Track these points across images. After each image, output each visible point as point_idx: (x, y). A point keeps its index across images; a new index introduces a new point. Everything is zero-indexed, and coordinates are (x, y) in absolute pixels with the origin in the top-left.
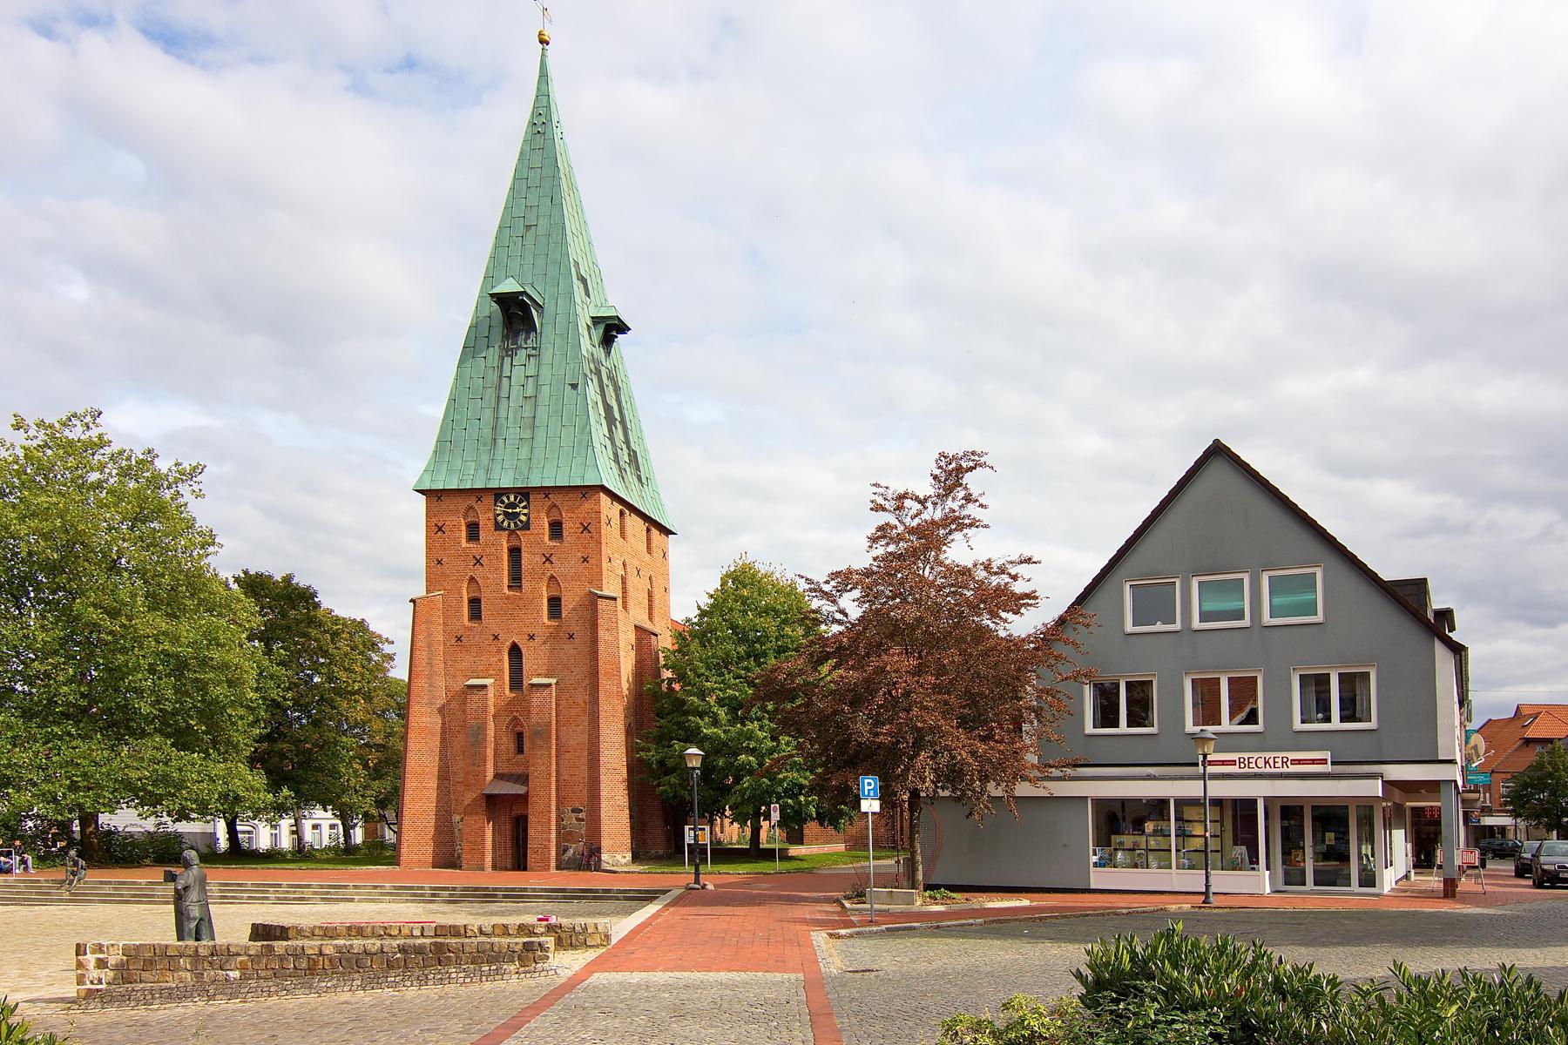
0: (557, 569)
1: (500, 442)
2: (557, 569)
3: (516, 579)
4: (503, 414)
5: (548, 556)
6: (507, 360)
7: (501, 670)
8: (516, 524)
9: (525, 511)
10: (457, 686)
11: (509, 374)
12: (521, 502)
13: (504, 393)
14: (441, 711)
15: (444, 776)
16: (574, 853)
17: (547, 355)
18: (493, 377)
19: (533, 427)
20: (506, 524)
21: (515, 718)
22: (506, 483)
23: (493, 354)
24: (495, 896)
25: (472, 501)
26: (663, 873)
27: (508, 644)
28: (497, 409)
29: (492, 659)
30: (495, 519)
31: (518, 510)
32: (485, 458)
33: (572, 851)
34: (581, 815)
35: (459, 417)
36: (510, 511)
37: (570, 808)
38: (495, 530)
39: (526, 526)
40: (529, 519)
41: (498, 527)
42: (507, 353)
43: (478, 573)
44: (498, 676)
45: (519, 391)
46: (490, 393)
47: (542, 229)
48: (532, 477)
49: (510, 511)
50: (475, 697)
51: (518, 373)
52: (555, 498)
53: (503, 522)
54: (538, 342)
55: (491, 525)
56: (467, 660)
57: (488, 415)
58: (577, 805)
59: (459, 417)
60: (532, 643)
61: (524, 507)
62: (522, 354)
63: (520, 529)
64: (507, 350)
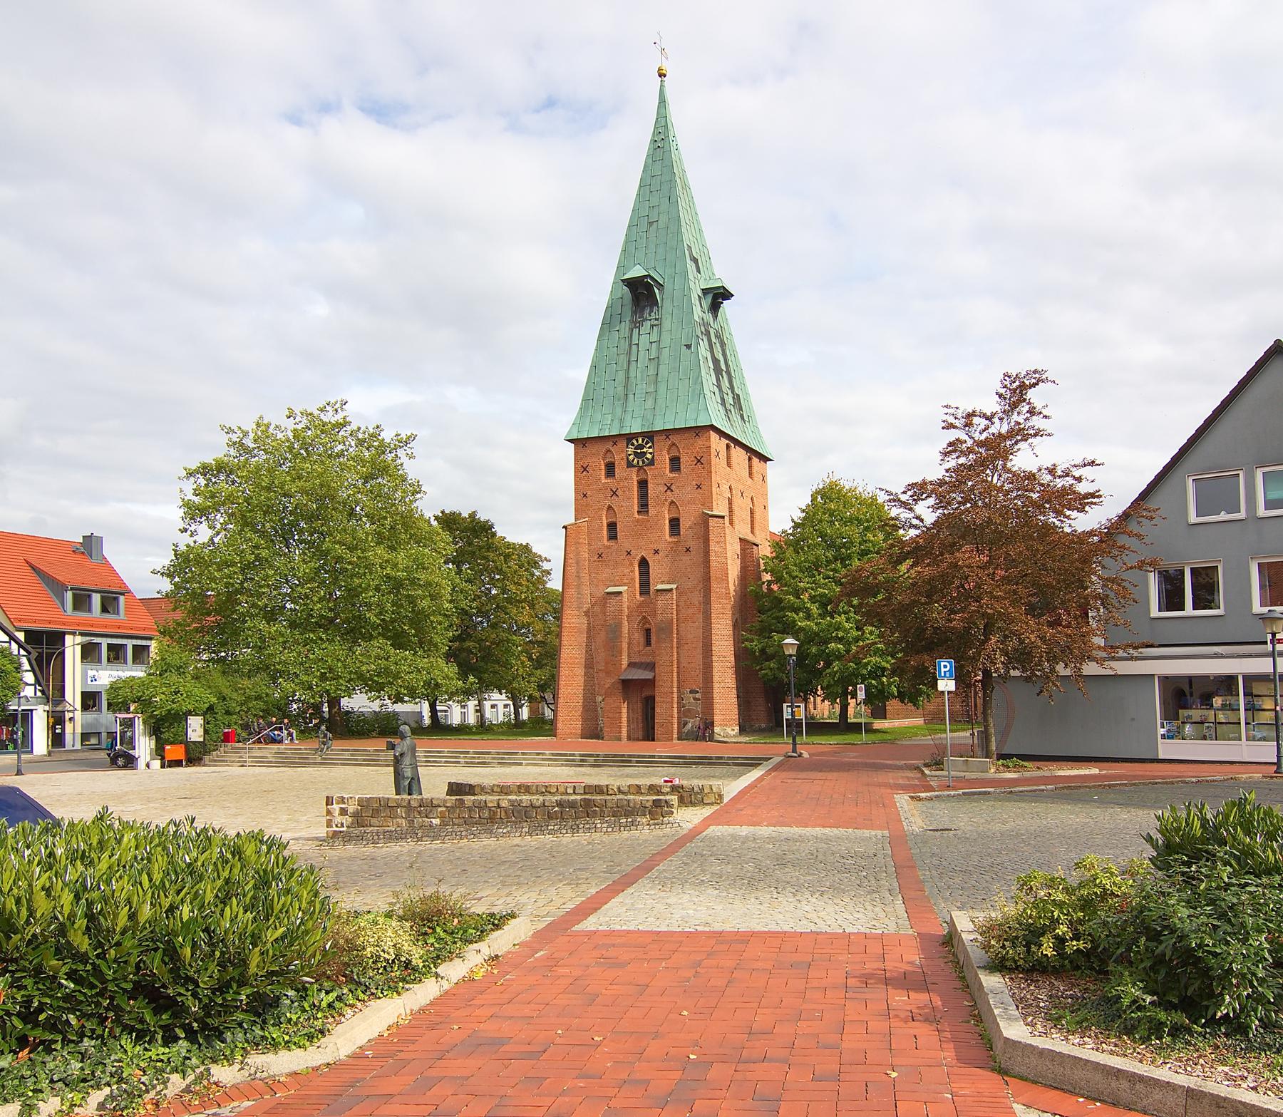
0: (676, 496)
2: (676, 496)
3: (644, 505)
4: (632, 374)
6: (636, 331)
7: (633, 579)
8: (643, 462)
9: (651, 450)
10: (599, 593)
12: (647, 443)
13: (633, 358)
14: (587, 613)
15: (589, 665)
17: (667, 324)
18: (624, 345)
20: (635, 462)
21: (644, 617)
22: (636, 428)
23: (625, 327)
24: (630, 762)
25: (609, 446)
26: (765, 743)
27: (638, 558)
29: (625, 571)
31: (645, 450)
32: (619, 411)
33: (690, 725)
34: (698, 696)
36: (639, 451)
39: (652, 462)
41: (630, 465)
43: (615, 503)
44: (630, 584)
45: (645, 354)
46: (623, 359)
49: (639, 451)
50: (613, 601)
51: (644, 340)
52: (673, 438)
55: (624, 463)
56: (606, 573)
58: (694, 687)
60: (657, 556)
61: (650, 447)
63: (647, 465)
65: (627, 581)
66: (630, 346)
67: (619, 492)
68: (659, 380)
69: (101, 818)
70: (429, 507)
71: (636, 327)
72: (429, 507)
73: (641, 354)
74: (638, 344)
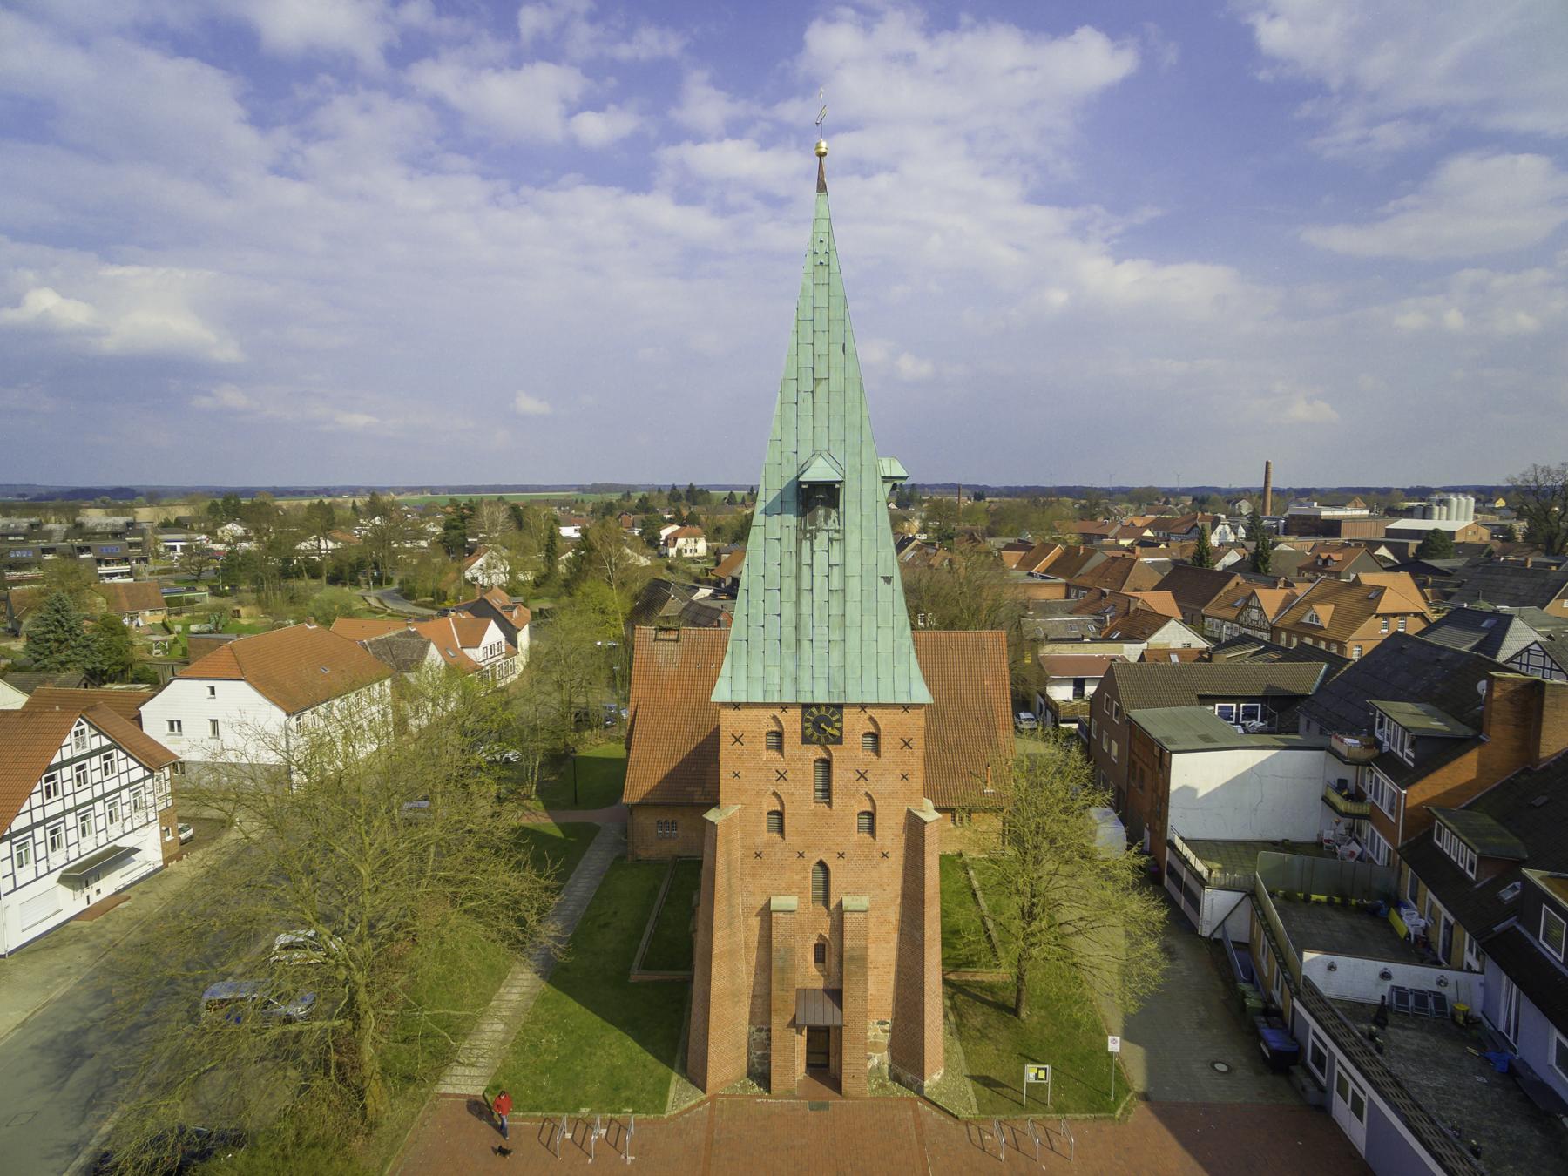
0: (872, 786)
1: (806, 644)
2: (872, 786)
3: (826, 792)
4: (806, 609)
5: (862, 772)
6: (806, 545)
11: (810, 562)
13: (805, 584)
16: (879, 1063)
17: (853, 540)
18: (790, 564)
19: (844, 627)
28: (798, 603)
30: (803, 732)
32: (789, 665)
33: (876, 1061)
35: (754, 611)
37: (876, 1021)
38: (803, 743)
40: (841, 734)
42: (805, 535)
43: (782, 789)
46: (789, 584)
47: (836, 378)
48: (849, 689)
51: (820, 559)
53: (812, 735)
54: (842, 523)
57: (788, 611)
58: (884, 1018)
59: (754, 611)
60: (842, 861)
62: (822, 538)
64: (805, 532)
65: (797, 890)
66: (799, 566)
67: (789, 775)
68: (847, 624)
69: (970, 138)
70: (1304, 973)
71: (806, 539)
72: (1304, 973)
73: (818, 580)
74: (811, 566)
